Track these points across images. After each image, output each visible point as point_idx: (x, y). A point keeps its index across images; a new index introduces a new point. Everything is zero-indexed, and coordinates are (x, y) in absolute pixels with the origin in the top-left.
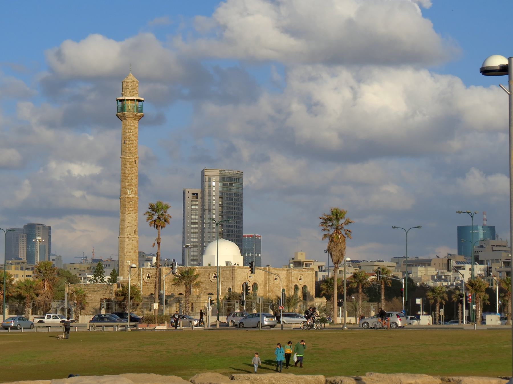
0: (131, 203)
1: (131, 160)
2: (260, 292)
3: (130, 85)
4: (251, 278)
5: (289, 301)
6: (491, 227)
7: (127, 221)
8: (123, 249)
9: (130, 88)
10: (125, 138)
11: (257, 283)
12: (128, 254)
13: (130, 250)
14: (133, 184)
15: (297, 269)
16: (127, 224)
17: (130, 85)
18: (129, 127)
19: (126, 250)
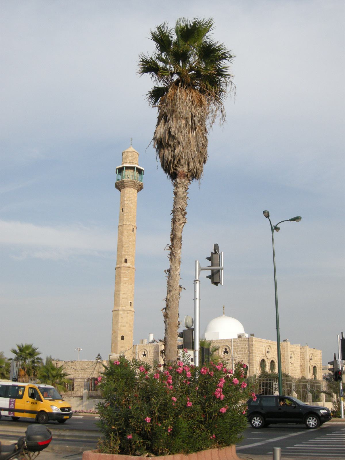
0: (127, 272)
1: (128, 228)
2: (223, 79)
3: (130, 155)
4: (313, 360)
5: (304, 362)
6: (68, 408)
7: (122, 292)
8: (117, 322)
9: (130, 158)
10: (124, 206)
11: (317, 367)
12: (122, 328)
13: (125, 324)
14: (130, 253)
15: (87, 433)
16: (122, 296)
17: (130, 155)
18: (128, 195)
19: (120, 324)
